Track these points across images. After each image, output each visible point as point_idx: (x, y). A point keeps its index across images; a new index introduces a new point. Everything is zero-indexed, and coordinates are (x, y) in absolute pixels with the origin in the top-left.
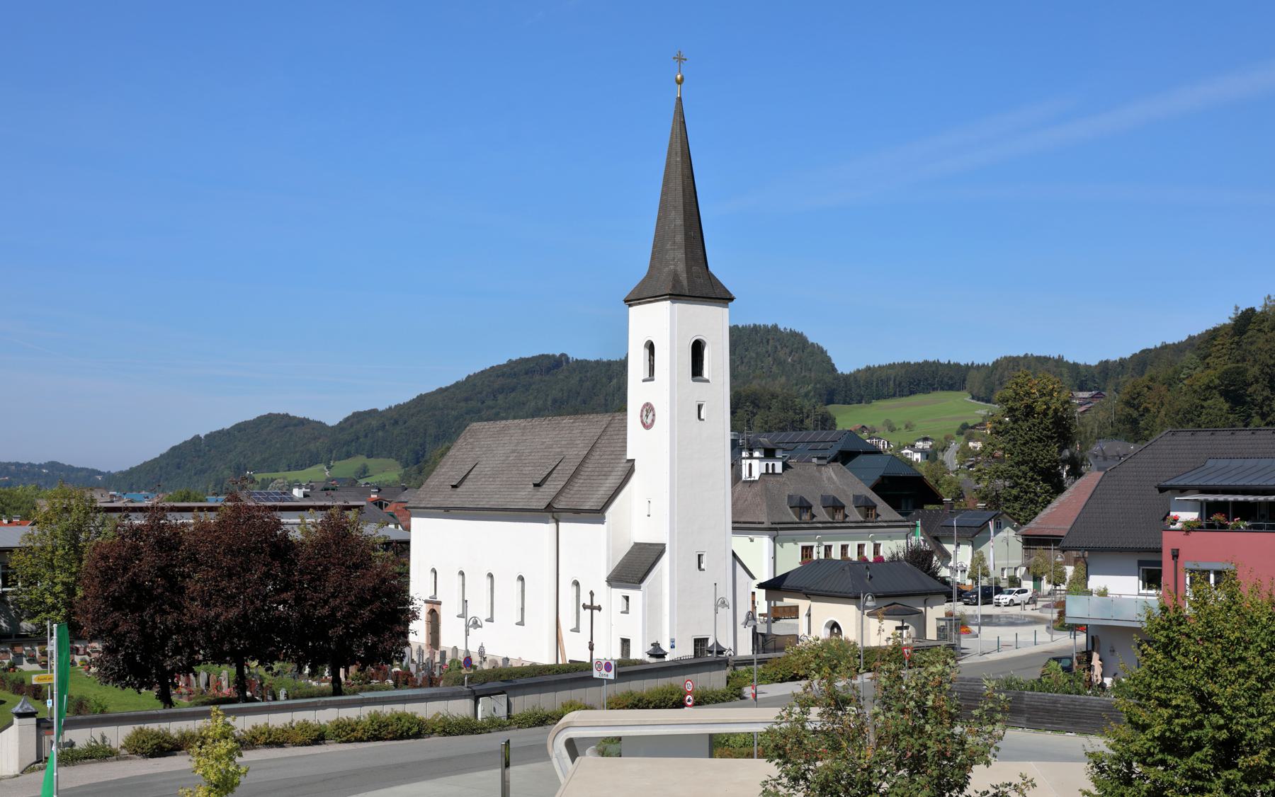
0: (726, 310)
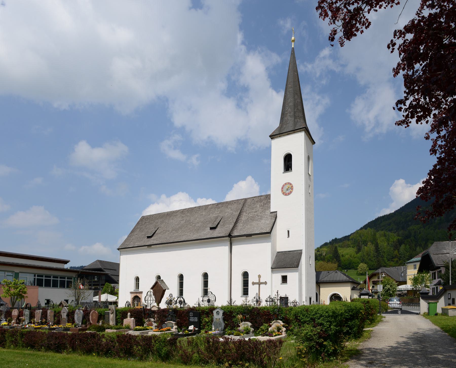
0: (278, 250)
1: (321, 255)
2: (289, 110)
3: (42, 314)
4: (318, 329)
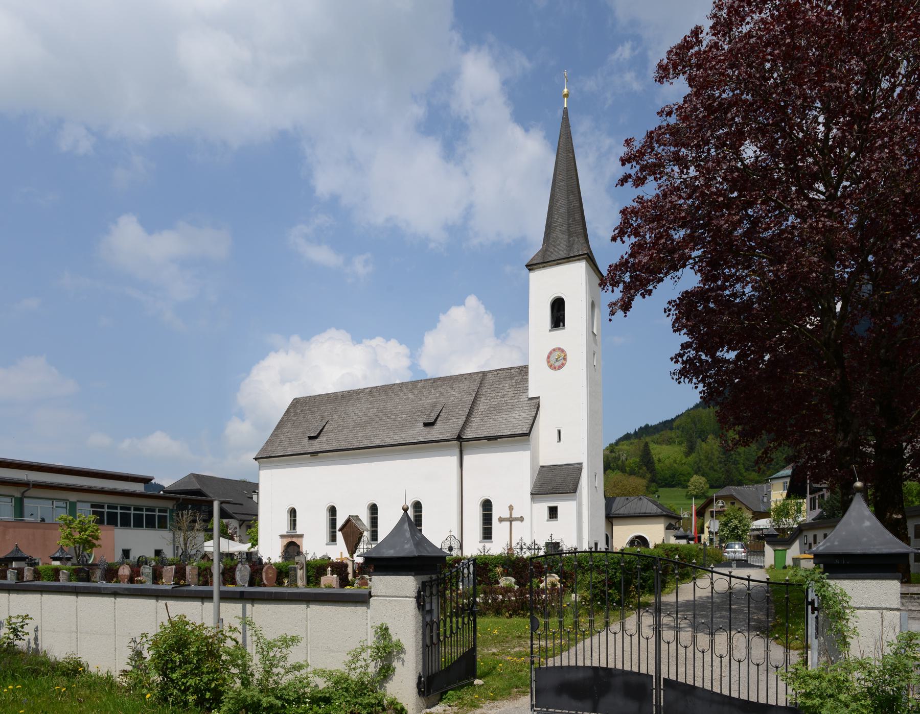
0: (542, 463)
1: (617, 458)
2: (560, 220)
3: (176, 572)
4: (603, 576)
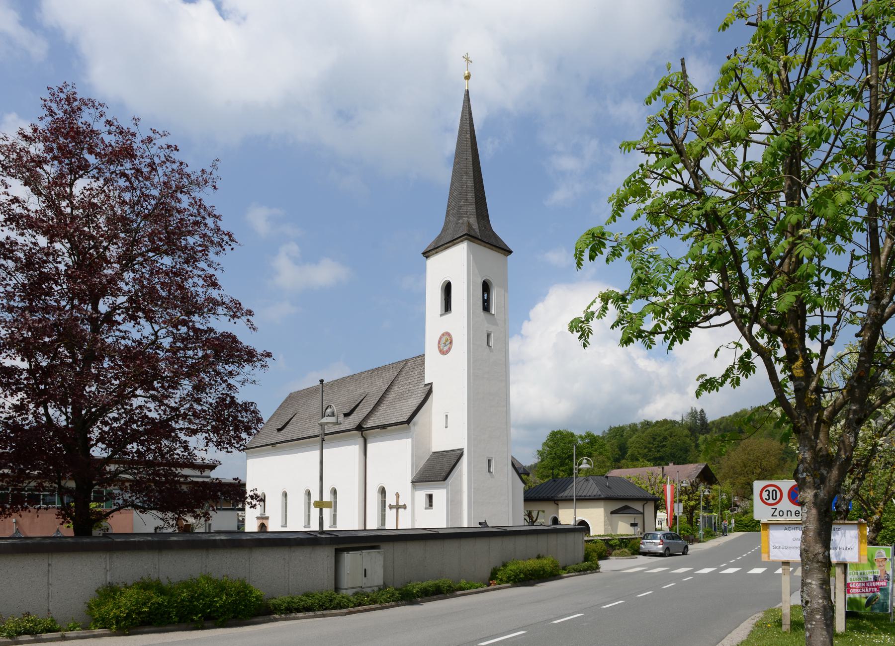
0: (434, 450)
